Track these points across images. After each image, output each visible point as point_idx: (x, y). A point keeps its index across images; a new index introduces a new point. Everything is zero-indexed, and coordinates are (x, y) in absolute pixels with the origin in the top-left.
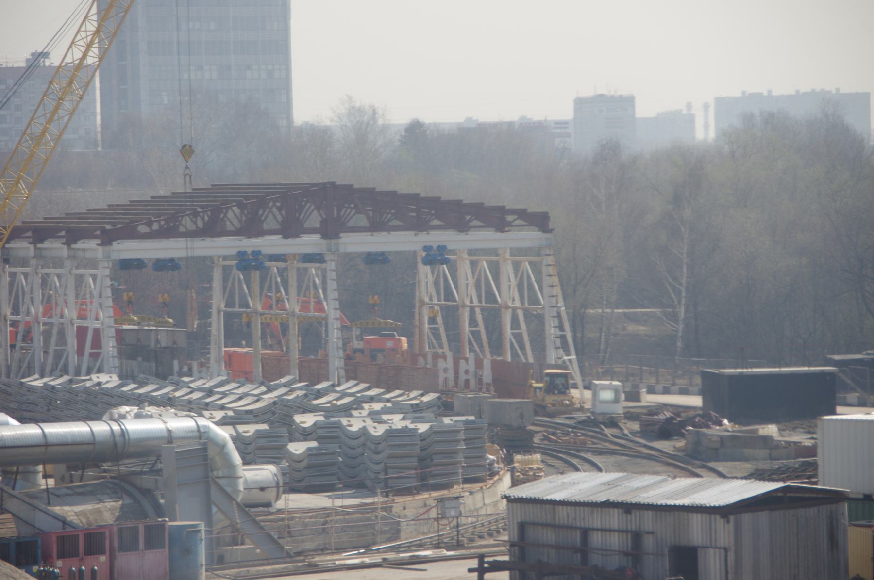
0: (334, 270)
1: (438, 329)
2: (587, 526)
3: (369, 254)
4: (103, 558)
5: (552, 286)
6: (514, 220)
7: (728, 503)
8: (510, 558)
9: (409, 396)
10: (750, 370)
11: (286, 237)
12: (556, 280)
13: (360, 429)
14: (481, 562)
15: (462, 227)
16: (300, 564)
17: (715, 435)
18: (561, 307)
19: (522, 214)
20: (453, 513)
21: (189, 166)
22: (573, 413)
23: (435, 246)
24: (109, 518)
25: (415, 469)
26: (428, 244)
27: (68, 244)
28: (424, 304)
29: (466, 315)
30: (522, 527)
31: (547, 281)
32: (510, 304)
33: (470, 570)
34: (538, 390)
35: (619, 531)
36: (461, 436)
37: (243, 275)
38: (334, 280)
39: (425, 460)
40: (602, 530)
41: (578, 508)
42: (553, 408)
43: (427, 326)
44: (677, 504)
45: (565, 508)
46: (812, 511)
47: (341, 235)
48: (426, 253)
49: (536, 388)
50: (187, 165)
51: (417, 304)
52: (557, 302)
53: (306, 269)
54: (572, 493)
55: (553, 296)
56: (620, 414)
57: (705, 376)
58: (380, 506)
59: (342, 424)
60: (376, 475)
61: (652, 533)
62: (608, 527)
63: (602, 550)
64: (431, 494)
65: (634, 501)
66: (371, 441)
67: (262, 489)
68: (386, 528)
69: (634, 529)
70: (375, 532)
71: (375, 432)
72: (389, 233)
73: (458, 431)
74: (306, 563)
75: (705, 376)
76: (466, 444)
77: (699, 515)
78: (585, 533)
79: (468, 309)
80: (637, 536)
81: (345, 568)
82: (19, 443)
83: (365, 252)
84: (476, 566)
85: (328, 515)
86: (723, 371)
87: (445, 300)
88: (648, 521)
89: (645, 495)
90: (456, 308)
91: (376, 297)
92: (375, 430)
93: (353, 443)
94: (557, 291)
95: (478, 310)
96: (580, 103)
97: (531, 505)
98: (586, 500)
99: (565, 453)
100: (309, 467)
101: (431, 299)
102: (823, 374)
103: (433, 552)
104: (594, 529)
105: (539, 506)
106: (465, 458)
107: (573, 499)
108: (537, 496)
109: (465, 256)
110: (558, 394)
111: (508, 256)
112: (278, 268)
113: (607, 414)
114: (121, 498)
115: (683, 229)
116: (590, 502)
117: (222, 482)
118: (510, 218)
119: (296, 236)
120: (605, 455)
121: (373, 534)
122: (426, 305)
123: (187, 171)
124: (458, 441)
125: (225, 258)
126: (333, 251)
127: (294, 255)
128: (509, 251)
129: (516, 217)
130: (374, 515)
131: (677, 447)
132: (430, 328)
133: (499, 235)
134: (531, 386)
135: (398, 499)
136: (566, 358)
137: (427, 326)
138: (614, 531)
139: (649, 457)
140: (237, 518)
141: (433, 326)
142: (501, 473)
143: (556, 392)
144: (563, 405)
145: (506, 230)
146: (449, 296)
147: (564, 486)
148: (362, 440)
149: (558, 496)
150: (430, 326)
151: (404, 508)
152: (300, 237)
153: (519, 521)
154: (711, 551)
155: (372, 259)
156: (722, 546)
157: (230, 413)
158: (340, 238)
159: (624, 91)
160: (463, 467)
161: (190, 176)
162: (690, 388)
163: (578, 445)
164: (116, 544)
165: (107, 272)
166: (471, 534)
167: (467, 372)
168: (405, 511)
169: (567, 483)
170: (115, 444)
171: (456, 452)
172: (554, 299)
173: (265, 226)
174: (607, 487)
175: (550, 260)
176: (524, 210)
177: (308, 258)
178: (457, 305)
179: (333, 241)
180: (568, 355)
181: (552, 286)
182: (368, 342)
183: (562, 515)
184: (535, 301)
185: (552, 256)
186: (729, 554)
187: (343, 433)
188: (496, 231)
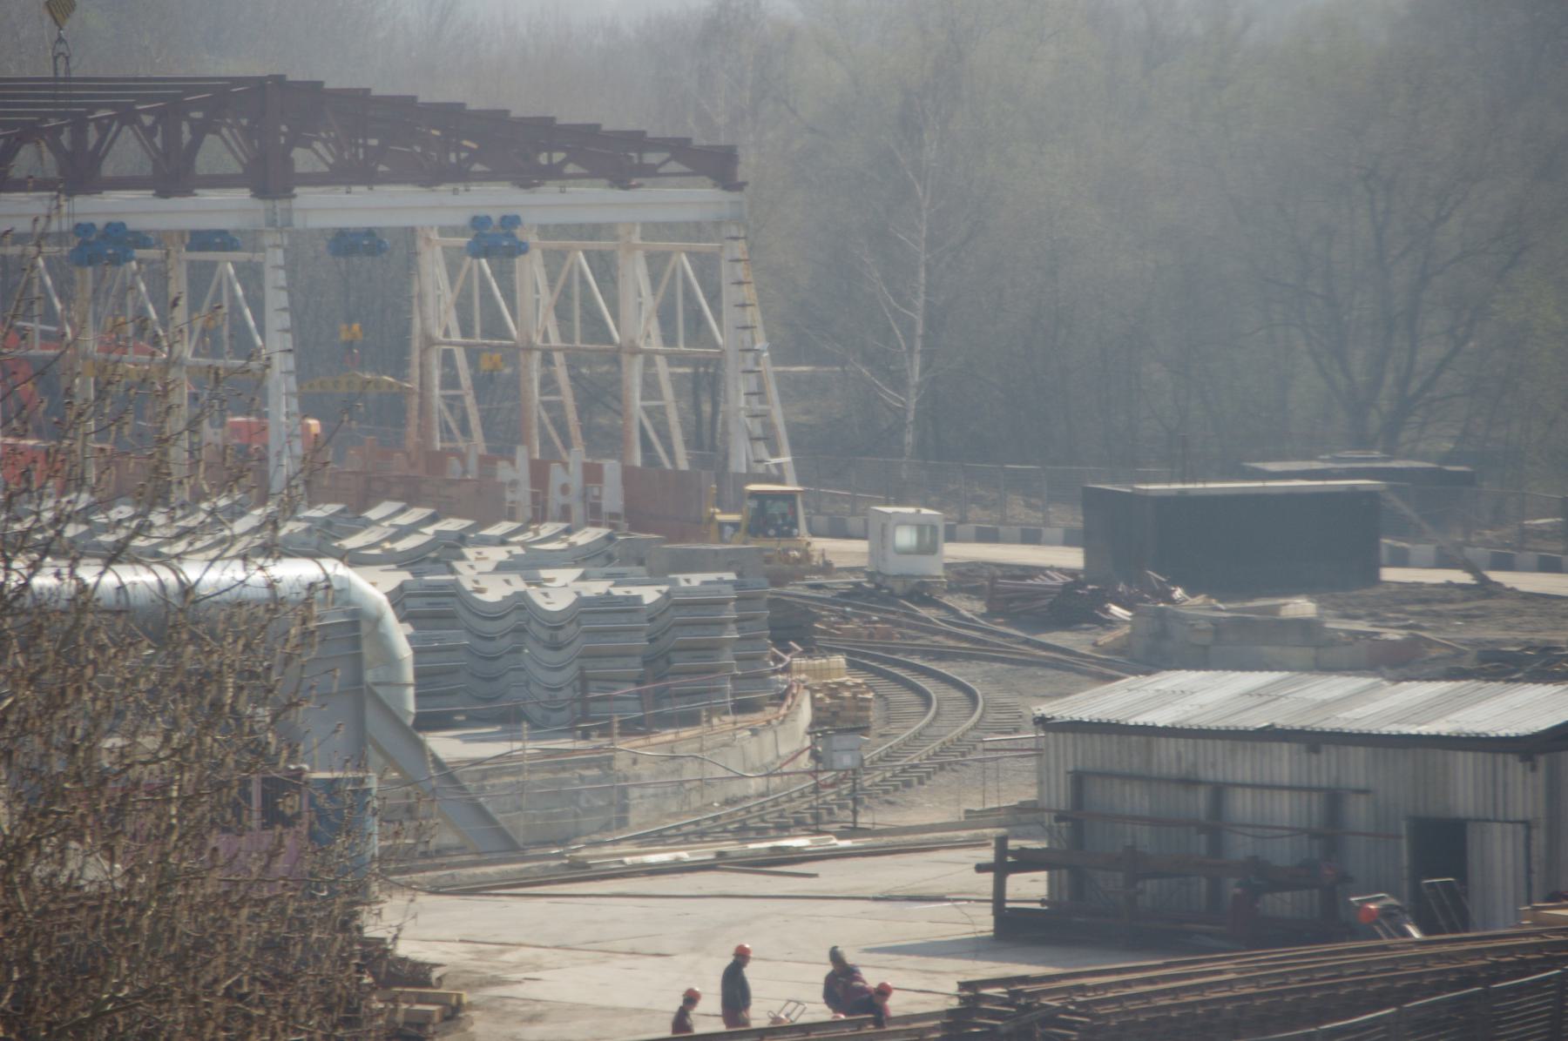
0: (281, 267)
1: (459, 398)
2: (1220, 778)
3: (341, 234)
5: (743, 306)
6: (663, 163)
7: (1535, 731)
8: (1050, 843)
9: (536, 532)
10: (1200, 486)
11: (163, 193)
12: (749, 293)
13: (505, 598)
15: (529, 177)
16: (553, 863)
17: (1201, 617)
18: (763, 351)
19: (680, 148)
20: (847, 760)
21: (63, 36)
22: (807, 577)
23: (495, 216)
25: (638, 683)
26: (482, 213)
28: (434, 344)
29: (534, 370)
30: (1079, 780)
31: (729, 294)
32: (642, 345)
34: (729, 529)
35: (1290, 788)
36: (730, 613)
38: (282, 288)
39: (657, 663)
40: (1253, 786)
41: (1200, 742)
42: (767, 566)
43: (437, 392)
44: (1424, 733)
45: (1172, 741)
47: (297, 190)
48: (476, 232)
49: (722, 525)
50: (59, 34)
51: (416, 344)
52: (753, 342)
53: (213, 265)
54: (1187, 712)
55: (745, 328)
56: (939, 577)
57: (1094, 502)
58: (526, 768)
59: (464, 589)
60: (553, 693)
61: (1365, 792)
62: (1267, 780)
63: (1253, 826)
64: (678, 733)
65: (1328, 726)
66: (537, 621)
68: (601, 803)
69: (1324, 784)
70: (578, 811)
71: (548, 603)
72: (371, 189)
73: (724, 602)
74: (566, 861)
75: (1094, 502)
76: (740, 629)
77: (1470, 755)
78: (1219, 791)
79: (537, 355)
80: (1334, 798)
81: (642, 872)
83: (335, 229)
86: (1144, 487)
87: (484, 334)
88: (1356, 768)
89: (1346, 714)
91: (356, 327)
92: (548, 600)
93: (489, 627)
95: (558, 358)
97: (1097, 737)
98: (1222, 725)
99: (875, 658)
101: (447, 333)
102: (1353, 495)
103: (812, 841)
104: (1236, 785)
105: (1115, 738)
106: (736, 660)
107: (1196, 722)
108: (1113, 718)
109: (434, 236)
110: (776, 536)
111: (636, 239)
112: (235, 264)
113: (913, 576)
115: (919, 189)
116: (1232, 729)
117: (380, 691)
118: (652, 158)
119: (187, 192)
120: (954, 660)
121: (576, 815)
122: (436, 347)
123: (61, 48)
124: (722, 624)
125: (444, 231)
126: (279, 223)
127: (182, 233)
128: (638, 229)
129: (666, 155)
130: (577, 775)
131: (1101, 643)
132: (443, 397)
134: (712, 518)
135: (624, 744)
137: (437, 392)
138: (1282, 788)
139: (1056, 665)
140: (431, 766)
141: (451, 392)
143: (772, 532)
145: (633, 183)
146: (495, 327)
147: (1163, 699)
148: (511, 621)
149: (1161, 717)
150: (443, 392)
151: (635, 762)
152: (195, 195)
153: (1071, 768)
154: (1497, 827)
155: (347, 243)
156: (1520, 816)
157: (518, 550)
158: (294, 196)
160: (734, 678)
161: (67, 58)
162: (1002, 529)
163: (895, 641)
166: (776, 815)
167: (565, 489)
168: (637, 768)
169: (1165, 692)
172: (747, 335)
173: (108, 169)
174: (1255, 700)
175: (739, 249)
176: (685, 142)
177: (202, 240)
178: (514, 347)
179: (280, 205)
181: (743, 306)
182: (236, 428)
183: (1167, 756)
185: (743, 241)
186: (1534, 832)
187: (470, 611)
188: (611, 186)
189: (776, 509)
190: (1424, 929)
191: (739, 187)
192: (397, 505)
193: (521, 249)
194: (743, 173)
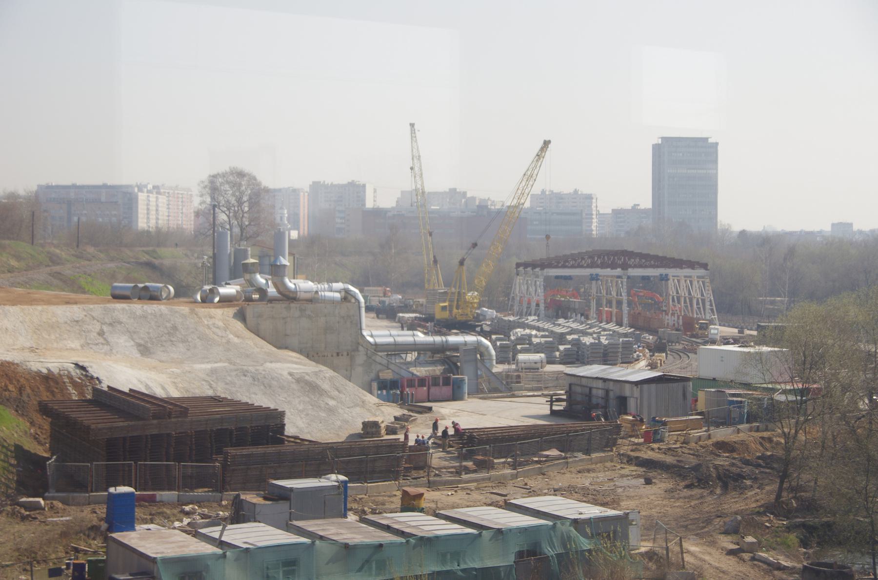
4: (425, 388)
14: (552, 398)
19: (698, 263)
23: (594, 274)
24: (438, 373)
27: (532, 269)
30: (570, 385)
31: (707, 288)
33: (547, 401)
37: (337, 282)
40: (596, 388)
46: (675, 385)
67: (536, 363)
78: (591, 389)
82: (404, 343)
84: (549, 400)
85: (559, 374)
88: (611, 386)
90: (679, 297)
94: (711, 292)
95: (687, 298)
96: (833, 225)
100: (565, 355)
109: (683, 278)
111: (696, 278)
114: (444, 365)
124: (619, 348)
133: (693, 271)
136: (713, 317)
142: (256, 383)
144: (704, 334)
149: (581, 374)
159: (849, 221)
164: (431, 383)
165: (542, 280)
167: (674, 321)
170: (443, 345)
171: (618, 352)
177: (619, 277)
180: (714, 315)
184: (704, 296)
189: (705, 325)
190: (605, 420)
191: (708, 270)
192: (579, 324)
193: (668, 280)
194: (709, 268)
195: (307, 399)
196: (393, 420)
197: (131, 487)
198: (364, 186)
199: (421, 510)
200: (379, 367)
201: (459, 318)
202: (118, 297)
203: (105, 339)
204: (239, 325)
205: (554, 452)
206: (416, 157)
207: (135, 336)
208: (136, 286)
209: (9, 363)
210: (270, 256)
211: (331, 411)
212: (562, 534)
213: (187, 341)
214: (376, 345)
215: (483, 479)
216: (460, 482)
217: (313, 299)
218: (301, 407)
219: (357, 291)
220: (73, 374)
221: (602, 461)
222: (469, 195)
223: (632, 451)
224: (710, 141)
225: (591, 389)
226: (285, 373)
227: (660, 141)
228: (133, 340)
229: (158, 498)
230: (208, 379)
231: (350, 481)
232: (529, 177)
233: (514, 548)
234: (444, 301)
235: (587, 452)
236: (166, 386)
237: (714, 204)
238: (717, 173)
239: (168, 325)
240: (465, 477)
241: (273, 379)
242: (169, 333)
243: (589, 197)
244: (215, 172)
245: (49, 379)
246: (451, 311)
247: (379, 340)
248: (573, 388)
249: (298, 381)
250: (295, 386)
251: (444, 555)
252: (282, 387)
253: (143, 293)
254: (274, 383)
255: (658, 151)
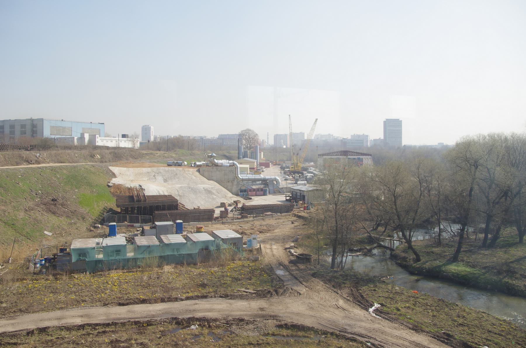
78: (297, 193)
88: (302, 192)
195: (207, 196)
196: (233, 202)
197: (171, 221)
198: (304, 133)
199: (202, 232)
200: (241, 186)
201: (297, 170)
202: (169, 165)
203: (155, 178)
204: (197, 173)
205: (269, 213)
206: (290, 124)
207: (164, 177)
208: (174, 162)
209: (120, 184)
210: (254, 153)
211: (213, 199)
212: (217, 243)
213: (179, 178)
214: (242, 179)
215: (241, 221)
216: (233, 222)
217: (222, 166)
218: (204, 198)
219: (237, 163)
220: (137, 188)
221: (286, 216)
222: (334, 135)
223: (297, 213)
224: (400, 120)
225: (297, 193)
226: (202, 188)
227: (385, 120)
228: (163, 178)
229: (134, 226)
230: (178, 189)
231: (184, 222)
232: (313, 129)
233: (199, 247)
234: (293, 165)
235: (281, 213)
236: (164, 191)
237: (401, 138)
238: (402, 129)
239: (175, 173)
240: (235, 221)
241: (197, 189)
242: (174, 176)
243: (367, 136)
244: (243, 130)
245: (130, 189)
246: (294, 168)
247: (244, 178)
248: (293, 192)
249: (205, 190)
250: (204, 192)
251: (173, 250)
252: (200, 192)
253: (177, 164)
254: (198, 191)
255: (385, 122)
